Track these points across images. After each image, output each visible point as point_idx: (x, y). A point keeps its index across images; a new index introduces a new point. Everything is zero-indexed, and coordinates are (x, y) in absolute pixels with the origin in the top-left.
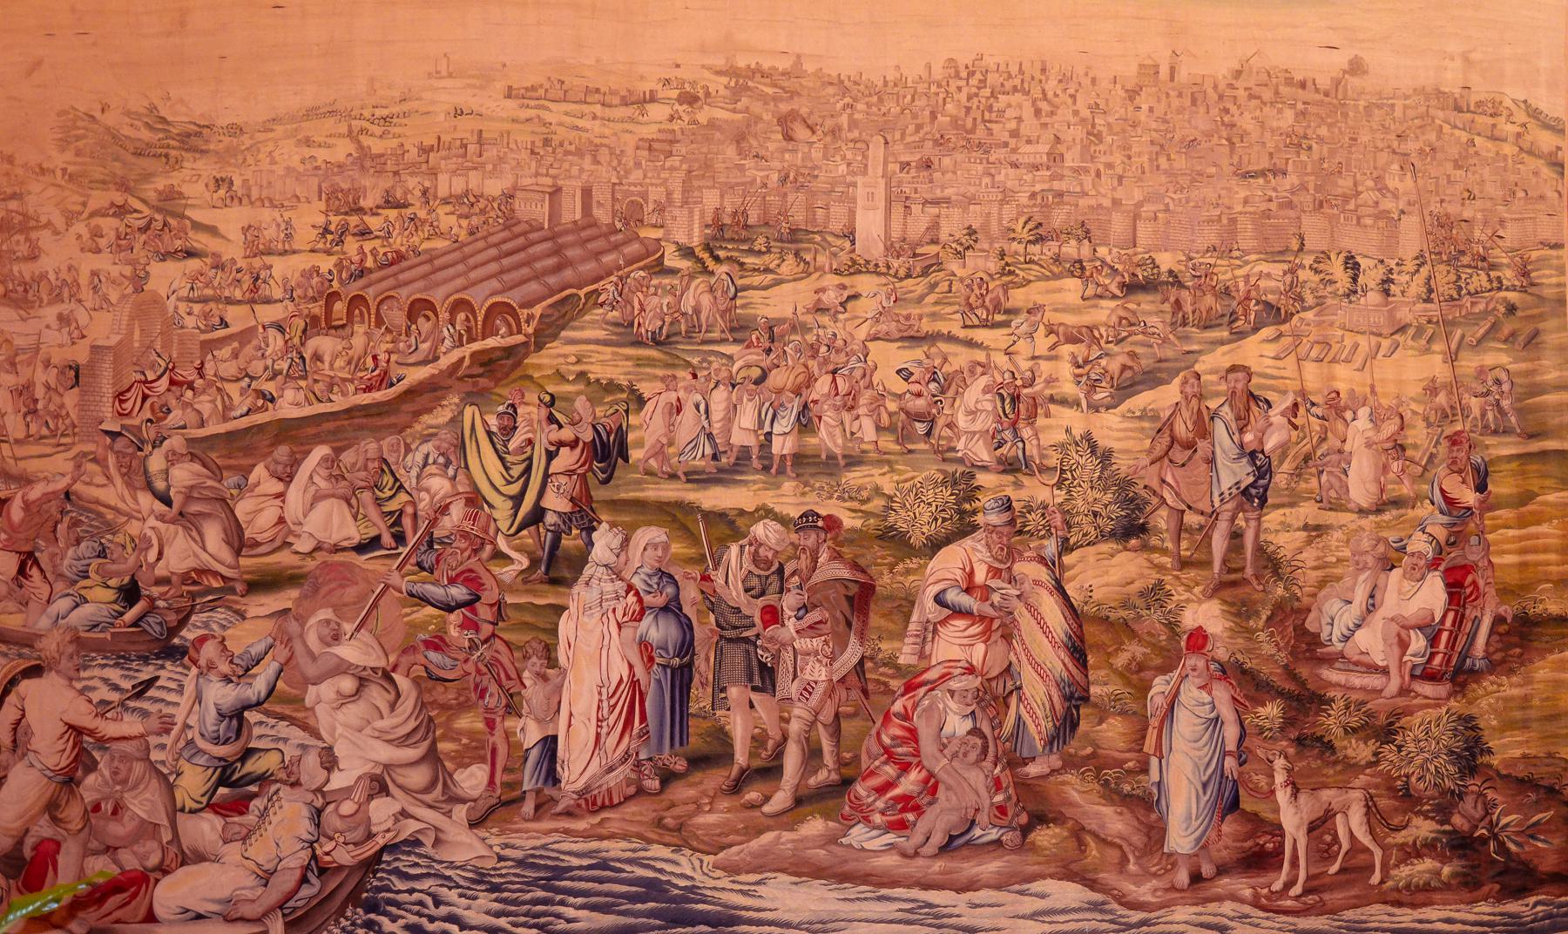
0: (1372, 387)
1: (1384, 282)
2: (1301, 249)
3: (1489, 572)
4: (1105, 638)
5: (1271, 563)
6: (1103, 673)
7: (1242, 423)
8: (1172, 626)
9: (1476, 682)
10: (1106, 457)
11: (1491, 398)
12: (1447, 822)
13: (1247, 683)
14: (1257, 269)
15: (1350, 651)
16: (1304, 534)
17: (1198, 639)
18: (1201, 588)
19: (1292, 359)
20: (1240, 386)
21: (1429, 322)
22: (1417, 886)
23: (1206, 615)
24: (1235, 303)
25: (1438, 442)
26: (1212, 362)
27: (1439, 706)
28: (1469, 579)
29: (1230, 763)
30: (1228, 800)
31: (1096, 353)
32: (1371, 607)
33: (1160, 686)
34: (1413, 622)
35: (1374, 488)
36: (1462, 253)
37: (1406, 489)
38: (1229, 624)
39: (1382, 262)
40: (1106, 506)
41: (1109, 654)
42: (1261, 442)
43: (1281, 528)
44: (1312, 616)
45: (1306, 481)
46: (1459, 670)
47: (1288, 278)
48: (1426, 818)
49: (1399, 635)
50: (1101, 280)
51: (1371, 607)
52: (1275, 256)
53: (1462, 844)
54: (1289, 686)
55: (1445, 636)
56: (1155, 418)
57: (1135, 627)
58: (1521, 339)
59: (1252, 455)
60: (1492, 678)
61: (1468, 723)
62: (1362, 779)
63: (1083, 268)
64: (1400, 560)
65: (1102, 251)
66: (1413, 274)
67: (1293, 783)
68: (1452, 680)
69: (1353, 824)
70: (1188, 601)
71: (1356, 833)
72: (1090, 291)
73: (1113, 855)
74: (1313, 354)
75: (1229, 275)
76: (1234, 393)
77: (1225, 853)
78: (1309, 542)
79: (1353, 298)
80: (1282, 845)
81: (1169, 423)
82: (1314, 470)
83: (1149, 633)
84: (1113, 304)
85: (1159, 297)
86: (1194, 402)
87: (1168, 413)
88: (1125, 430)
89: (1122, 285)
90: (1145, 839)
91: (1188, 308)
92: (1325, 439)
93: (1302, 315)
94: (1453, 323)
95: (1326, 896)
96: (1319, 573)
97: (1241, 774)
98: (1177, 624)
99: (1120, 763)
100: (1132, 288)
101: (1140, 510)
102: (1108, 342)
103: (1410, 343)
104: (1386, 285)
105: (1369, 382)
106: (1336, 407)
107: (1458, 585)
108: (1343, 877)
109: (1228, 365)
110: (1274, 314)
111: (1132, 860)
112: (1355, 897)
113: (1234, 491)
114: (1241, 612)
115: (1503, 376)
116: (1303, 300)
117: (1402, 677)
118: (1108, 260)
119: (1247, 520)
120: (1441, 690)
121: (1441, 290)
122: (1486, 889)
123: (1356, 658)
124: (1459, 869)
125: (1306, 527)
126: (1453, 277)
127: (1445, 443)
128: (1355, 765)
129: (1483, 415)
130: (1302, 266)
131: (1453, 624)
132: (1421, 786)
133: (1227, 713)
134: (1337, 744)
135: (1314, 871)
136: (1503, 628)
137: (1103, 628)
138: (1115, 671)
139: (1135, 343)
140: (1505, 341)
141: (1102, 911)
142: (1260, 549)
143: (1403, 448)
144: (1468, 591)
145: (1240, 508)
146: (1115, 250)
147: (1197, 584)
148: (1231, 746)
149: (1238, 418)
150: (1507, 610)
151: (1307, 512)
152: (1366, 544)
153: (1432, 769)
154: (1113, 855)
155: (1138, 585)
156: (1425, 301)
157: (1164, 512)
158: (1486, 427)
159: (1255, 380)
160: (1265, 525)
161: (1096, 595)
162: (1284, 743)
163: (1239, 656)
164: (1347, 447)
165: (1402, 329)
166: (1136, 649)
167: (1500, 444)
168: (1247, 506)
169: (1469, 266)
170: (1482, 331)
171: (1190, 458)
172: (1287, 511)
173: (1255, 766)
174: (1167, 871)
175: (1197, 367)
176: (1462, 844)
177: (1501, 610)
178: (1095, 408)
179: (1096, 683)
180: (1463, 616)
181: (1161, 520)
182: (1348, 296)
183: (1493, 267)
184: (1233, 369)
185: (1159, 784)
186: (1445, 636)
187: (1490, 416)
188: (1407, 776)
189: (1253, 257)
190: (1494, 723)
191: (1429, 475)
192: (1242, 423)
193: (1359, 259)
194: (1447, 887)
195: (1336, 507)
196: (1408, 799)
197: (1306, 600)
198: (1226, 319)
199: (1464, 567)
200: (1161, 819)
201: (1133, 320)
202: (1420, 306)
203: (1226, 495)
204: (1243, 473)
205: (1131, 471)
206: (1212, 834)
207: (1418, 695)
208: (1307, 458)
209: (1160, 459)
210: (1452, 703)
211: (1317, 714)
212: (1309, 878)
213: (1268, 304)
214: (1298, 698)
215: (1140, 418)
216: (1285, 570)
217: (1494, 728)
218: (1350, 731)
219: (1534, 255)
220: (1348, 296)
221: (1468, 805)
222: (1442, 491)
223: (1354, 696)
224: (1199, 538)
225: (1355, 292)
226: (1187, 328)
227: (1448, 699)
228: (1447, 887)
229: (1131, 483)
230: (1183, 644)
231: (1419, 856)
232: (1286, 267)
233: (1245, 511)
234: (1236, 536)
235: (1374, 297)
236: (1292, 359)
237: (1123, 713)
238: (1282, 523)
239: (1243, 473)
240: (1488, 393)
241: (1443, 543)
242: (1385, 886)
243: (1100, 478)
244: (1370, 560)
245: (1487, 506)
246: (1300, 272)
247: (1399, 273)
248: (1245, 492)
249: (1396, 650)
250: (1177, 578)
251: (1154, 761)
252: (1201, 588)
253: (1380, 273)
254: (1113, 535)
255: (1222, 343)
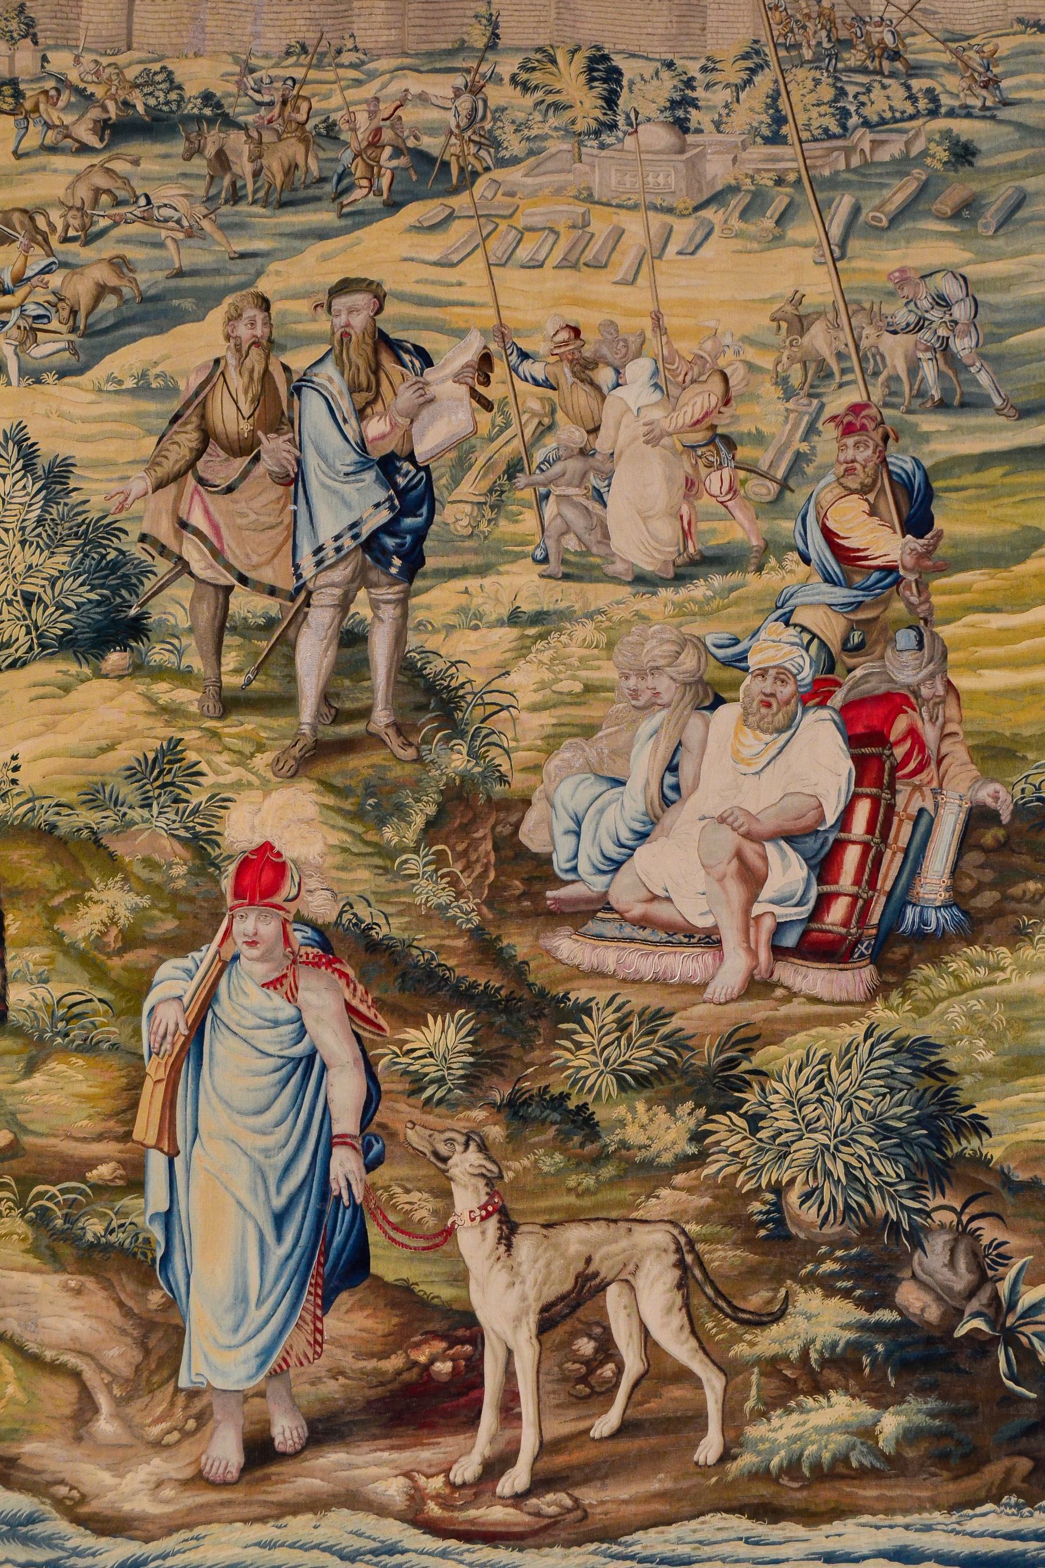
0: (657, 318)
1: (674, 105)
2: (493, 45)
3: (952, 711)
4: (46, 874)
5: (432, 699)
6: (34, 955)
7: (362, 398)
8: (201, 846)
9: (935, 960)
10: (57, 478)
11: (926, 335)
12: (886, 1300)
13: (391, 976)
14: (395, 87)
15: (624, 892)
16: (513, 633)
17: (263, 874)
18: (269, 756)
19: (476, 264)
20: (359, 321)
21: (779, 182)
22: (816, 1466)
23: (279, 815)
24: (347, 156)
25: (811, 430)
26: (317, 266)
27: (849, 1019)
28: (901, 725)
29: (345, 1164)
30: (335, 1259)
31: (38, 260)
32: (670, 795)
33: (174, 982)
34: (768, 824)
35: (667, 531)
36: (847, 44)
37: (739, 529)
38: (335, 838)
39: (670, 65)
40: (53, 582)
41: (53, 913)
42: (407, 436)
43: (461, 623)
44: (532, 816)
45: (514, 518)
46: (888, 935)
47: (465, 103)
48: (830, 1291)
49: (739, 855)
50: (54, 116)
51: (670, 795)
52: (435, 61)
53: (917, 1357)
54: (485, 978)
55: (852, 855)
56: (169, 391)
57: (118, 847)
58: (991, 216)
59: (387, 466)
60: (975, 952)
61: (921, 1057)
62: (667, 1199)
63: (18, 95)
64: (735, 685)
65: (60, 61)
66: (739, 88)
67: (503, 1212)
68: (876, 958)
69: (647, 1310)
70: (238, 785)
71: (658, 1334)
72: (31, 141)
73: (61, 1394)
74: (523, 253)
75: (336, 101)
76: (345, 335)
77: (332, 1388)
78: (522, 651)
79: (607, 138)
80: (475, 1366)
81: (199, 401)
82: (528, 494)
83: (149, 863)
84: (81, 163)
85: (179, 147)
86: (255, 357)
87: (195, 382)
88: (101, 419)
89: (103, 127)
90: (136, 1356)
91: (244, 167)
92: (550, 428)
93: (497, 174)
94: (833, 183)
95: (589, 1495)
96: (547, 718)
97: (369, 1189)
98: (212, 838)
99: (79, 1168)
100: (119, 130)
101: (133, 589)
102: (66, 240)
103: (736, 223)
104: (679, 113)
105: (651, 307)
106: (584, 362)
107: (874, 737)
108: (625, 1445)
109: (335, 279)
110: (428, 175)
111: (103, 1401)
112: (661, 1496)
113: (348, 543)
114: (370, 807)
115: (952, 289)
116: (497, 144)
117: (753, 953)
118: (73, 76)
119: (375, 604)
120: (849, 981)
121: (802, 118)
122: (994, 1471)
123: (637, 910)
124: (921, 1420)
125: (514, 618)
126: (827, 93)
127: (830, 432)
128: (647, 1165)
129: (914, 368)
130: (495, 78)
131: (870, 829)
132: (810, 1214)
133: (334, 1042)
134: (601, 1114)
135: (558, 1427)
136: (990, 836)
137: (41, 851)
138: (69, 950)
139: (126, 240)
140: (956, 216)
141: (28, 1540)
142: (409, 671)
143: (730, 443)
144: (899, 752)
145: (360, 579)
146: (87, 58)
147: (261, 748)
148: (346, 1122)
149: (354, 388)
150: (999, 795)
151: (522, 584)
152: (655, 651)
153: (839, 1171)
154: (61, 1394)
155: (126, 754)
156: (768, 141)
157: (183, 591)
158: (921, 394)
159: (391, 308)
160: (418, 615)
161: (29, 778)
162: (479, 1114)
163: (362, 911)
164: (602, 443)
165: (717, 198)
166: (112, 902)
167: (954, 430)
168: (374, 575)
169: (864, 70)
170: (899, 199)
171: (245, 474)
172: (472, 583)
173: (403, 1171)
174: (186, 1435)
175: (264, 286)
176: (917, 1357)
177: (985, 794)
178: (34, 375)
179: (23, 978)
180: (891, 808)
181: (174, 607)
182: (597, 133)
183: (915, 70)
184: (345, 287)
185: (168, 1218)
186: (852, 855)
187: (929, 371)
188: (778, 1190)
189: (383, 64)
190: (986, 1058)
191: (796, 499)
192: (362, 398)
193: (618, 61)
194: (892, 1466)
195: (576, 571)
196: (774, 1240)
197: (519, 781)
198: (329, 188)
199: (887, 697)
200: (171, 1303)
201: (122, 194)
202: (760, 151)
203: (329, 553)
204: (366, 503)
205: (113, 505)
206: (298, 1341)
207: (792, 995)
208: (513, 469)
209: (178, 477)
210: (879, 1012)
211: (551, 1043)
212: (546, 1448)
213: (421, 157)
214: (508, 1006)
215: (132, 392)
216: (471, 715)
217: (987, 1072)
218: (634, 1083)
219: (1006, 45)
220: (597, 133)
221: (934, 1257)
222: (828, 534)
223: (638, 1000)
224: (264, 645)
225: (613, 126)
226: (243, 207)
227: (869, 1000)
228: (892, 1466)
229: (114, 531)
230: (227, 884)
231: (819, 1388)
232: (459, 80)
233: (371, 585)
234: (351, 640)
235: (656, 136)
236: (476, 264)
237: (89, 1048)
238: (462, 610)
239: (366, 503)
240: (920, 325)
241: (835, 647)
242: (734, 1468)
243: (40, 521)
244: (664, 685)
245: (932, 565)
246: (490, 91)
247: (708, 86)
248: (371, 545)
249: (736, 891)
250: (214, 734)
251: (157, 1162)
252: (269, 756)
253: (666, 87)
254: (67, 644)
255: (322, 234)
